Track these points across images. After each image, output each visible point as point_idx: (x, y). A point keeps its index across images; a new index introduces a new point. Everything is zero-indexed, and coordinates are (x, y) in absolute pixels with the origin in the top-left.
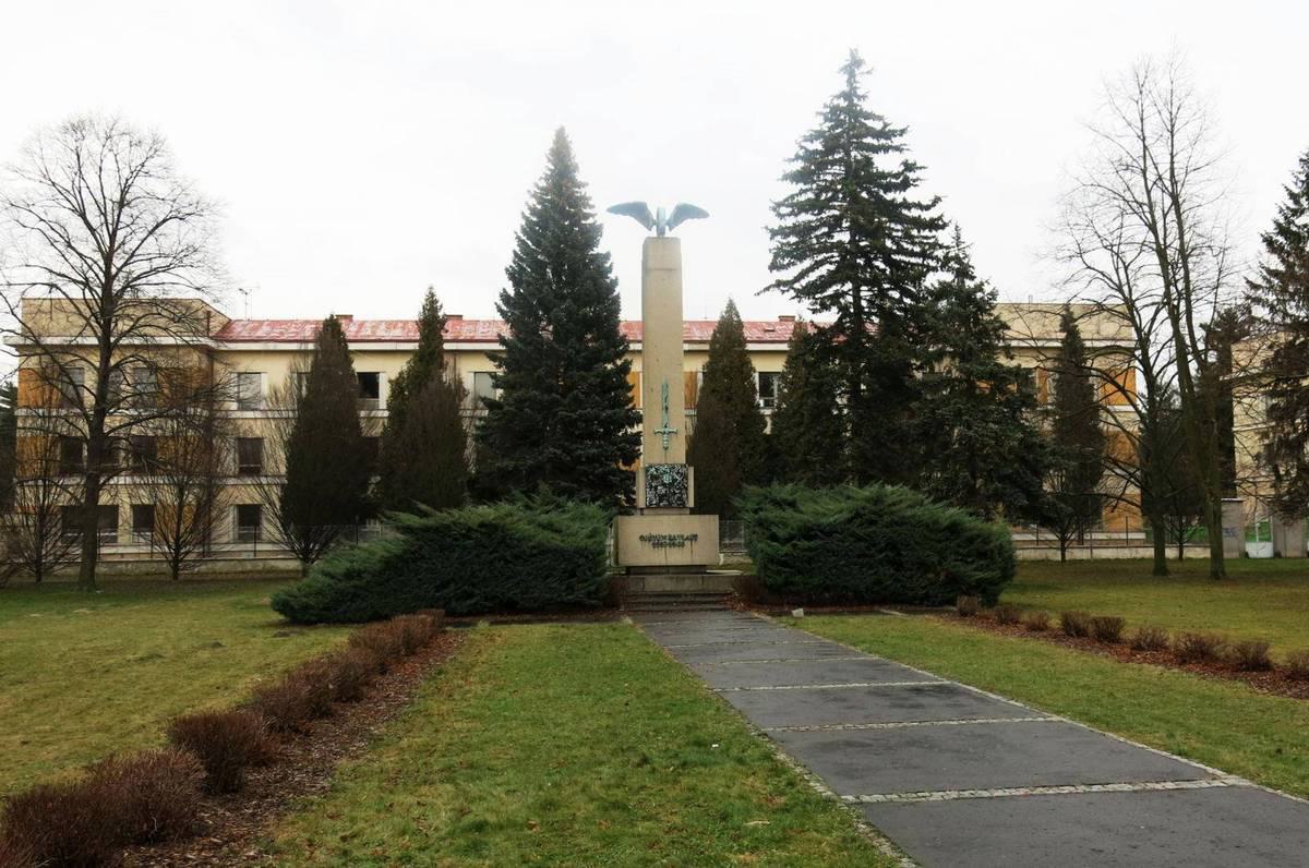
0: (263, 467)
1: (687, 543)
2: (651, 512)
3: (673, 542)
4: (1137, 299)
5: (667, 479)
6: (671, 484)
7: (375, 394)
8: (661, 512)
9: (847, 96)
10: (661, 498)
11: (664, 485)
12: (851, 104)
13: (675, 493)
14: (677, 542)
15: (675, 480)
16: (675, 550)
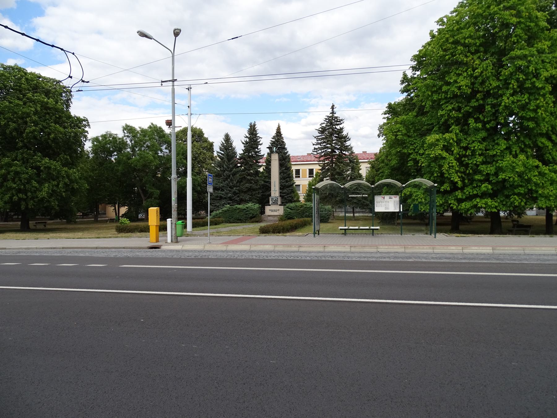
5: (274, 199)
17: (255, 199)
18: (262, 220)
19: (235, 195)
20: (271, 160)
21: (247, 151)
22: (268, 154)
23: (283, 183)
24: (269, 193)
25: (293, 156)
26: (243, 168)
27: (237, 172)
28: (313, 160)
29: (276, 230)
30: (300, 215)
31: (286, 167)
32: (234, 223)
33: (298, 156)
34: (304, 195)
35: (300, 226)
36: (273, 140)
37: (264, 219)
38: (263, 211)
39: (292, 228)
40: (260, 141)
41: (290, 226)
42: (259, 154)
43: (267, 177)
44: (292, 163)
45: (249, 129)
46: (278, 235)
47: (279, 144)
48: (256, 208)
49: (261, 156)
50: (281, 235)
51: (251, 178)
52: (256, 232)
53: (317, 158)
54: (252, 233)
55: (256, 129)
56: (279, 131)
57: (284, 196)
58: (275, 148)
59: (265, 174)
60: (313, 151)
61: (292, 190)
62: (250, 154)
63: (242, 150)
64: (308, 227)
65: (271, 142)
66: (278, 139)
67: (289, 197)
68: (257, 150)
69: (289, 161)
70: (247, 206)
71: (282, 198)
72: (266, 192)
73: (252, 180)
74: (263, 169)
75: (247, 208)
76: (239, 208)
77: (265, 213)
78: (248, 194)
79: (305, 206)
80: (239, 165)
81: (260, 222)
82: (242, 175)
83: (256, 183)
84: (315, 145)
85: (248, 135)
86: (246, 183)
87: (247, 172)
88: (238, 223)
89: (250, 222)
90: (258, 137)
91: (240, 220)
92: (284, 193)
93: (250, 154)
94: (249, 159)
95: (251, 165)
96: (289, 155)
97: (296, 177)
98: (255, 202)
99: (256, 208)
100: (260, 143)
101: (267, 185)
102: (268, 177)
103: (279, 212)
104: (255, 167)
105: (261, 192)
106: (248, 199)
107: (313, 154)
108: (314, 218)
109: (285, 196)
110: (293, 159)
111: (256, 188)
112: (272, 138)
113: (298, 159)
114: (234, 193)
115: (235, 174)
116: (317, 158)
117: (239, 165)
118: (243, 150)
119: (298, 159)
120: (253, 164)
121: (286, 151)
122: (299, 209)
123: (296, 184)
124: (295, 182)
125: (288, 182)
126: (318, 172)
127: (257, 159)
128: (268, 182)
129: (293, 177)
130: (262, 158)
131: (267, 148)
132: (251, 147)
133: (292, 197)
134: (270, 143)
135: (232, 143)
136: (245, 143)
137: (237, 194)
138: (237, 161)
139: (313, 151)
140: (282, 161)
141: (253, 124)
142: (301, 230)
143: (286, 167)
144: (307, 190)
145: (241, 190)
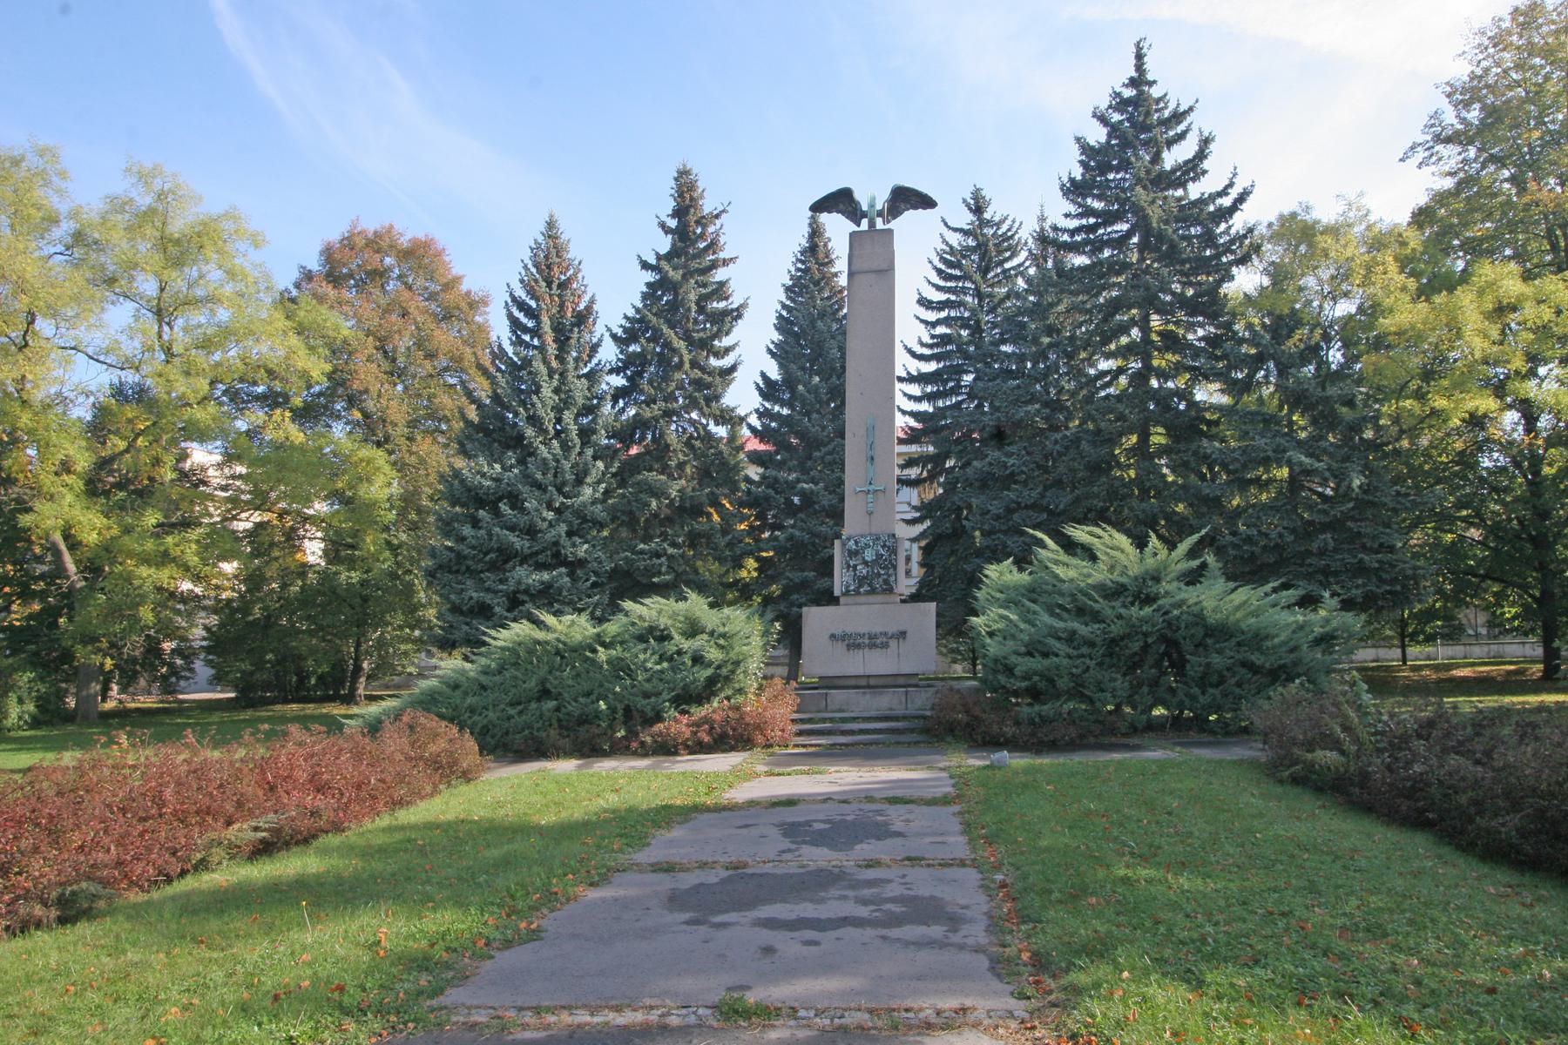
0: (1413, 327)
1: (893, 643)
3: (875, 642)
5: (869, 555)
8: (862, 599)
9: (1133, 83)
10: (861, 581)
11: (866, 563)
12: (1141, 93)
13: (879, 575)
15: (879, 556)
16: (877, 652)
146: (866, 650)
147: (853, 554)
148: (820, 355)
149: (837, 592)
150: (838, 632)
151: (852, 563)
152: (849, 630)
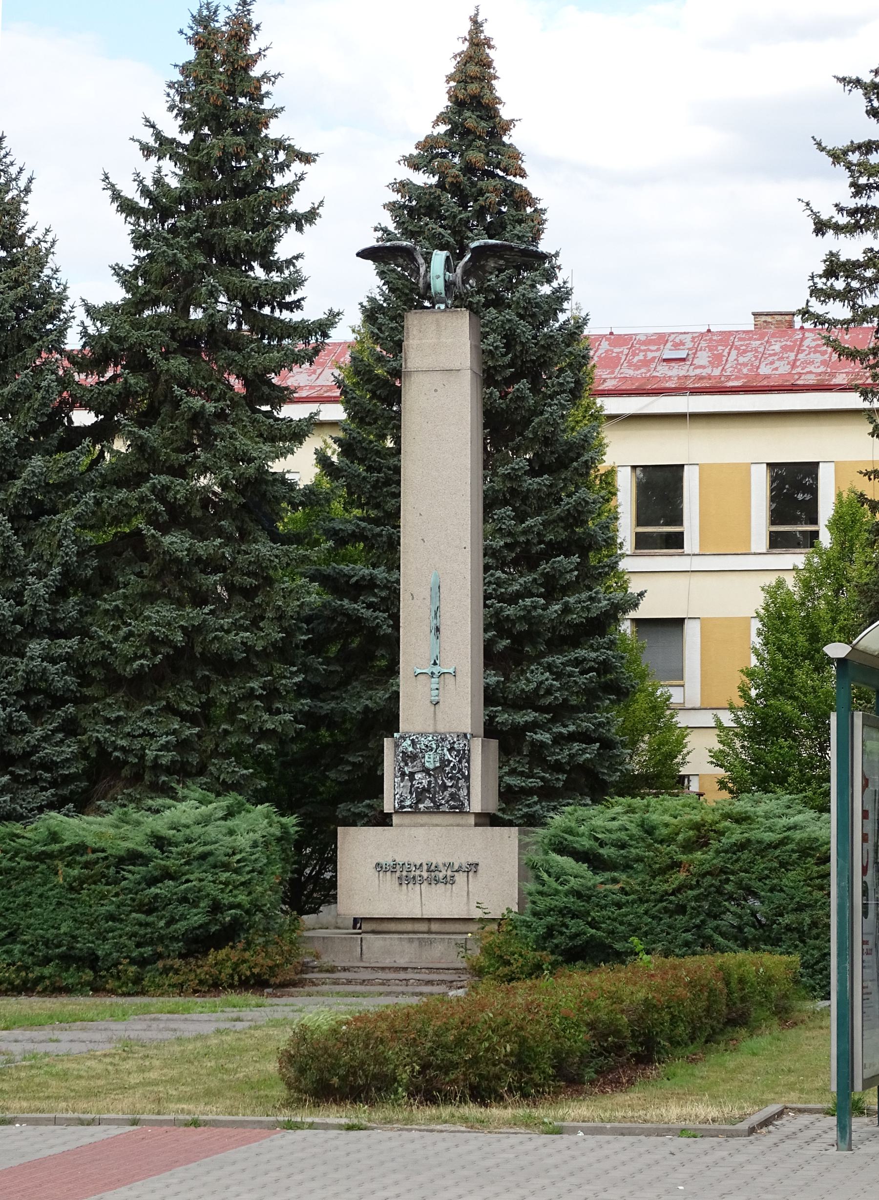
1: (460, 878)
2: (407, 819)
4: (435, 725)
5: (431, 761)
6: (440, 769)
7: (490, 238)
8: (425, 819)
10: (421, 794)
11: (426, 771)
13: (444, 787)
14: (441, 875)
15: (444, 763)
17: (238, 753)
18: (306, 968)
19: (36, 713)
20: (397, 373)
21: (164, 281)
22: (372, 313)
23: (512, 599)
24: (381, 695)
25: (615, 339)
26: (120, 445)
27: (68, 485)
28: (811, 380)
29: (448, 1067)
30: (681, 920)
31: (547, 441)
32: (26, 988)
33: (661, 339)
34: (727, 719)
35: (682, 1030)
36: (421, 179)
37: (327, 960)
38: (316, 879)
39: (605, 1051)
40: (291, 189)
41: (591, 1026)
42: (286, 315)
43: (357, 536)
44: (612, 406)
45: (185, 69)
46: (476, 1125)
47: (480, 214)
48: (243, 841)
49: (303, 330)
50: (514, 1122)
51: (204, 548)
52: (250, 1084)
53: (852, 355)
54: (210, 1095)
55: (256, 72)
56: (474, 88)
57: (519, 731)
58: (439, 257)
59: (337, 506)
60: (815, 292)
61: (604, 667)
62: (196, 314)
63: (118, 270)
64: (762, 1041)
65: (396, 197)
66: (469, 169)
67: (572, 737)
68: (259, 272)
69: (576, 392)
70: (158, 824)
71: (505, 751)
72: (344, 683)
73: (211, 565)
74: (322, 460)
75: (160, 842)
76: (80, 848)
77: (334, 899)
78: (170, 709)
79: (737, 834)
80: (83, 418)
81: (286, 986)
82: (116, 521)
83: (248, 593)
84: (838, 229)
85: (171, 127)
86: (150, 597)
87: (161, 493)
88: (67, 990)
89: (180, 989)
90: (279, 145)
91: (91, 961)
92: (527, 701)
93: (196, 314)
94: (179, 364)
95: (196, 418)
96: (580, 324)
97: (643, 542)
98: (236, 787)
99: (243, 841)
100: (299, 204)
101: (357, 621)
102: (370, 542)
103: (477, 884)
104: (243, 443)
105: (300, 691)
106: (166, 758)
107: (820, 320)
108: (846, 950)
109: (533, 726)
110: (612, 362)
111: (248, 648)
112: (414, 164)
113: (663, 370)
114: (27, 691)
115: (40, 510)
116: (852, 355)
117: (83, 418)
118: (125, 277)
119: (663, 370)
120: (221, 416)
121: (545, 289)
122: (676, 865)
123: (644, 611)
124: (634, 588)
125: (568, 589)
126: (862, 498)
127: (258, 360)
128: (368, 585)
129: (611, 542)
130: (310, 357)
131: (364, 254)
132: (207, 246)
133: (607, 744)
134: (393, 207)
135: (16, 203)
136: (144, 203)
137: (58, 701)
138: (65, 382)
139: (815, 292)
140: (511, 381)
141: (223, 16)
142: (701, 1069)
143: (547, 441)
144: (750, 674)
145: (103, 663)
146: (425, 886)
147: (408, 758)
148: (82, 666)
149: (388, 808)
150: (387, 860)
151: (407, 770)
152: (400, 860)
